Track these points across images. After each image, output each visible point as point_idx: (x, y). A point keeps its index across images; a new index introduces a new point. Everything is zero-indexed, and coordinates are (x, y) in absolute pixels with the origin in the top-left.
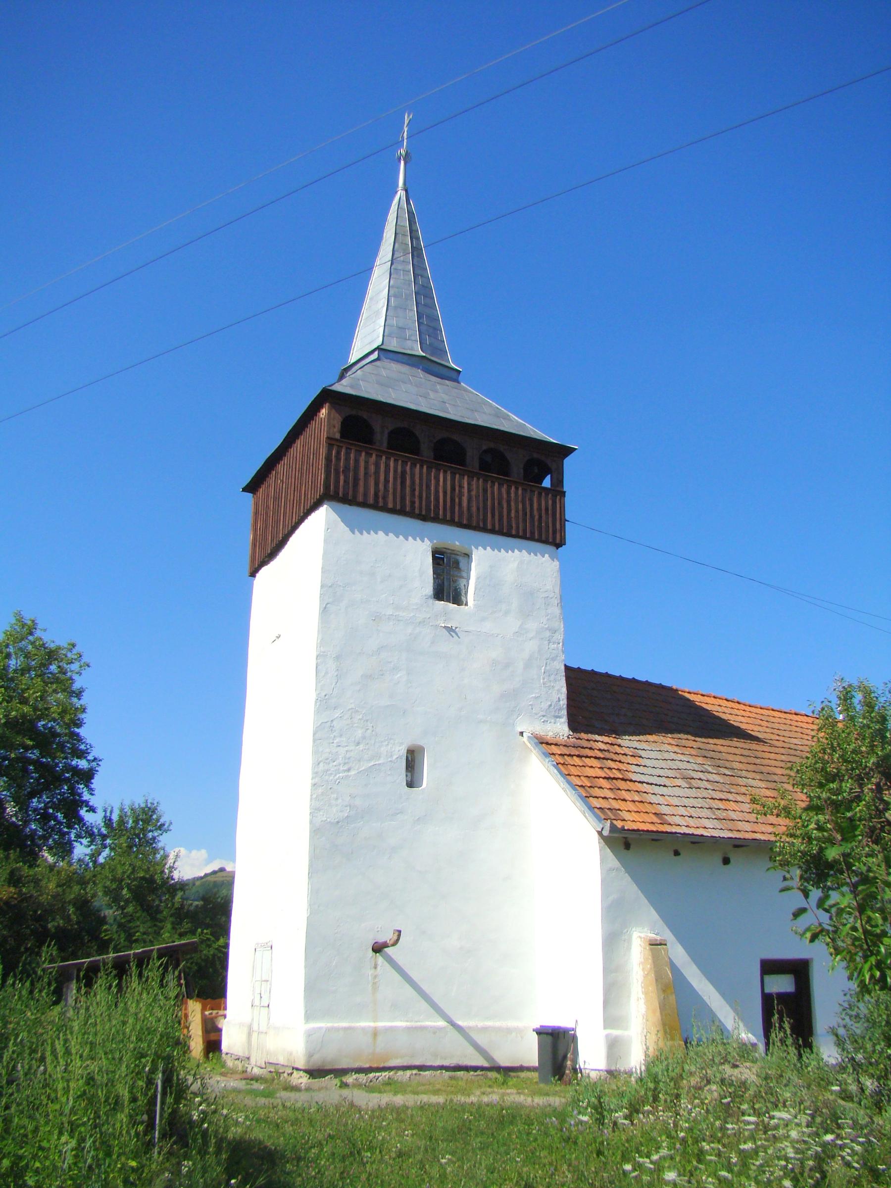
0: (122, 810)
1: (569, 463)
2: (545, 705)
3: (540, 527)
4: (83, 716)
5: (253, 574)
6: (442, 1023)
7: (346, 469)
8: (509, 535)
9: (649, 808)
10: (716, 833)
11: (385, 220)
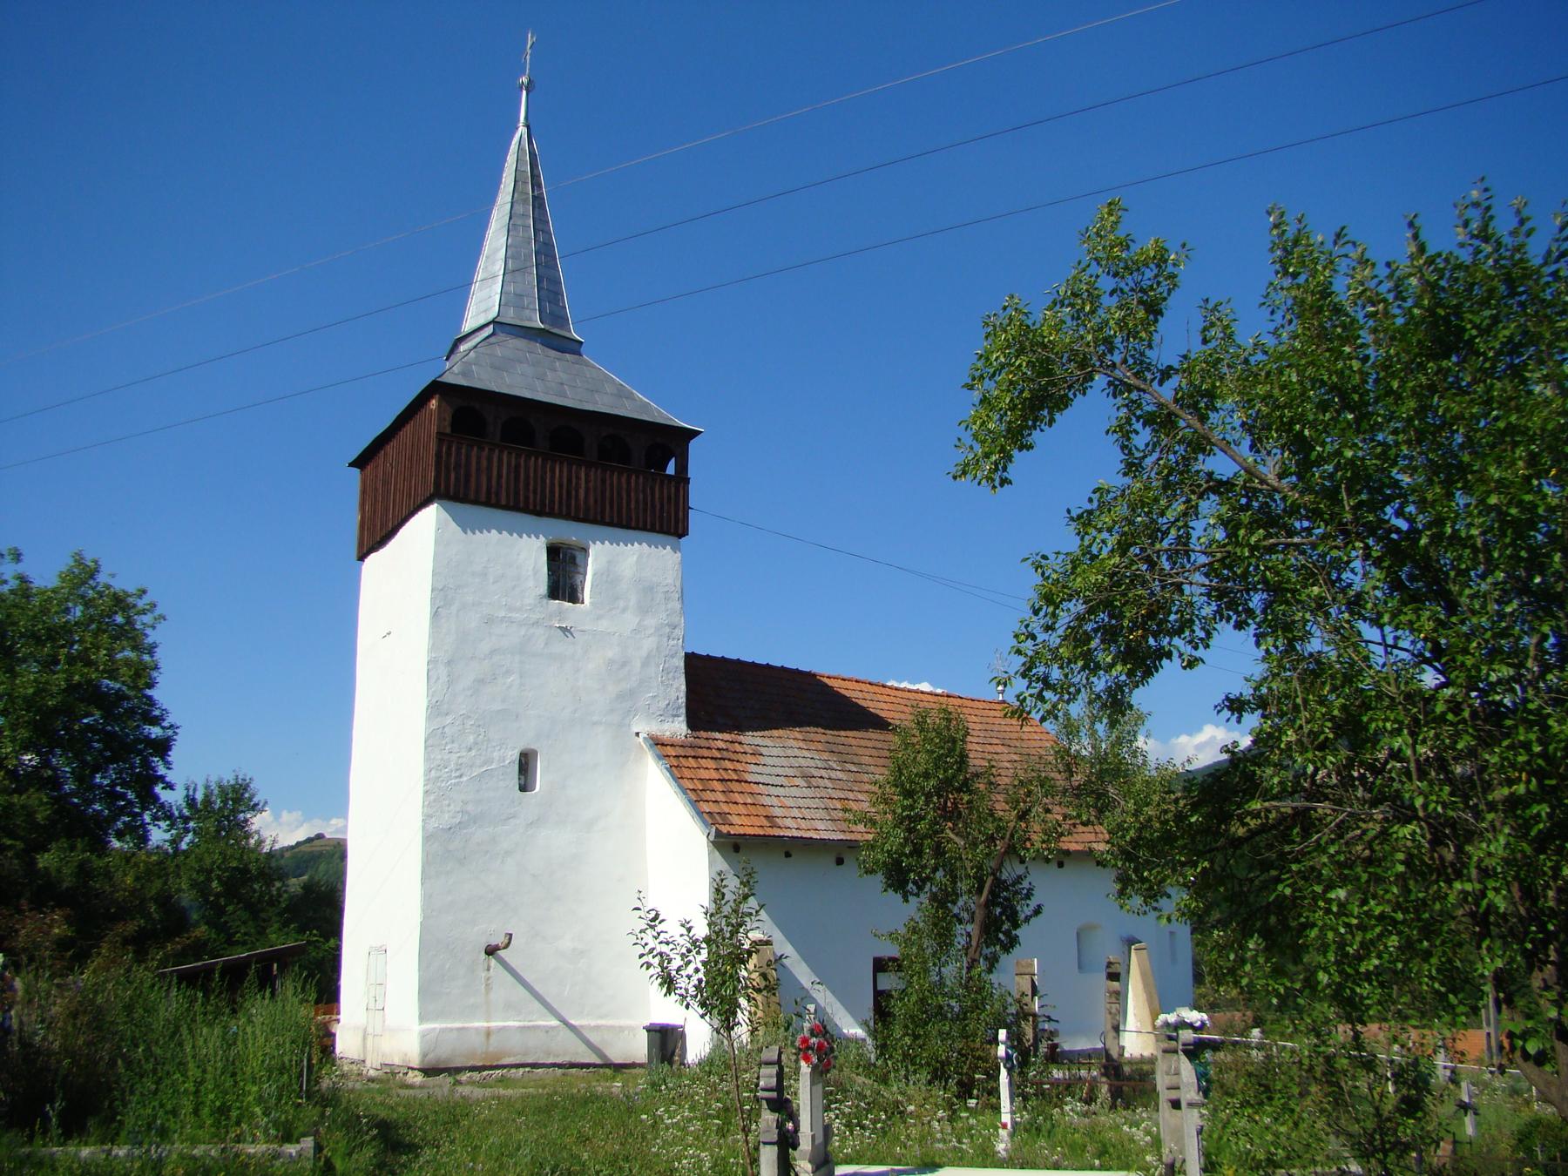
0: (207, 787)
1: (694, 445)
2: (663, 704)
3: (661, 517)
4: (155, 674)
5: (362, 558)
6: (555, 1022)
7: (458, 465)
8: (628, 527)
9: (761, 811)
10: (825, 835)
11: (505, 160)
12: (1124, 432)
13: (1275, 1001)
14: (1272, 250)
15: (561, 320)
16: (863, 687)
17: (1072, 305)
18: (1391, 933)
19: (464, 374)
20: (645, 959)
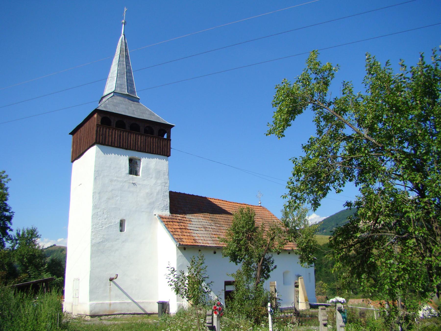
0: (23, 230)
1: (172, 129)
2: (163, 206)
4: (8, 196)
5: (73, 162)
6: (130, 301)
11: (117, 45)
12: (318, 122)
13: (370, 294)
14: (366, 66)
15: (134, 92)
16: (220, 201)
17: (302, 82)
18: (406, 273)
19: (105, 107)
20: (170, 283)
